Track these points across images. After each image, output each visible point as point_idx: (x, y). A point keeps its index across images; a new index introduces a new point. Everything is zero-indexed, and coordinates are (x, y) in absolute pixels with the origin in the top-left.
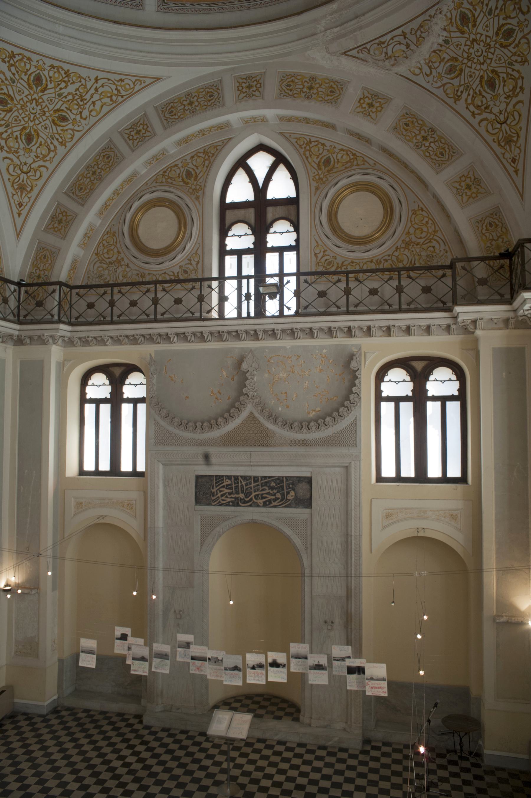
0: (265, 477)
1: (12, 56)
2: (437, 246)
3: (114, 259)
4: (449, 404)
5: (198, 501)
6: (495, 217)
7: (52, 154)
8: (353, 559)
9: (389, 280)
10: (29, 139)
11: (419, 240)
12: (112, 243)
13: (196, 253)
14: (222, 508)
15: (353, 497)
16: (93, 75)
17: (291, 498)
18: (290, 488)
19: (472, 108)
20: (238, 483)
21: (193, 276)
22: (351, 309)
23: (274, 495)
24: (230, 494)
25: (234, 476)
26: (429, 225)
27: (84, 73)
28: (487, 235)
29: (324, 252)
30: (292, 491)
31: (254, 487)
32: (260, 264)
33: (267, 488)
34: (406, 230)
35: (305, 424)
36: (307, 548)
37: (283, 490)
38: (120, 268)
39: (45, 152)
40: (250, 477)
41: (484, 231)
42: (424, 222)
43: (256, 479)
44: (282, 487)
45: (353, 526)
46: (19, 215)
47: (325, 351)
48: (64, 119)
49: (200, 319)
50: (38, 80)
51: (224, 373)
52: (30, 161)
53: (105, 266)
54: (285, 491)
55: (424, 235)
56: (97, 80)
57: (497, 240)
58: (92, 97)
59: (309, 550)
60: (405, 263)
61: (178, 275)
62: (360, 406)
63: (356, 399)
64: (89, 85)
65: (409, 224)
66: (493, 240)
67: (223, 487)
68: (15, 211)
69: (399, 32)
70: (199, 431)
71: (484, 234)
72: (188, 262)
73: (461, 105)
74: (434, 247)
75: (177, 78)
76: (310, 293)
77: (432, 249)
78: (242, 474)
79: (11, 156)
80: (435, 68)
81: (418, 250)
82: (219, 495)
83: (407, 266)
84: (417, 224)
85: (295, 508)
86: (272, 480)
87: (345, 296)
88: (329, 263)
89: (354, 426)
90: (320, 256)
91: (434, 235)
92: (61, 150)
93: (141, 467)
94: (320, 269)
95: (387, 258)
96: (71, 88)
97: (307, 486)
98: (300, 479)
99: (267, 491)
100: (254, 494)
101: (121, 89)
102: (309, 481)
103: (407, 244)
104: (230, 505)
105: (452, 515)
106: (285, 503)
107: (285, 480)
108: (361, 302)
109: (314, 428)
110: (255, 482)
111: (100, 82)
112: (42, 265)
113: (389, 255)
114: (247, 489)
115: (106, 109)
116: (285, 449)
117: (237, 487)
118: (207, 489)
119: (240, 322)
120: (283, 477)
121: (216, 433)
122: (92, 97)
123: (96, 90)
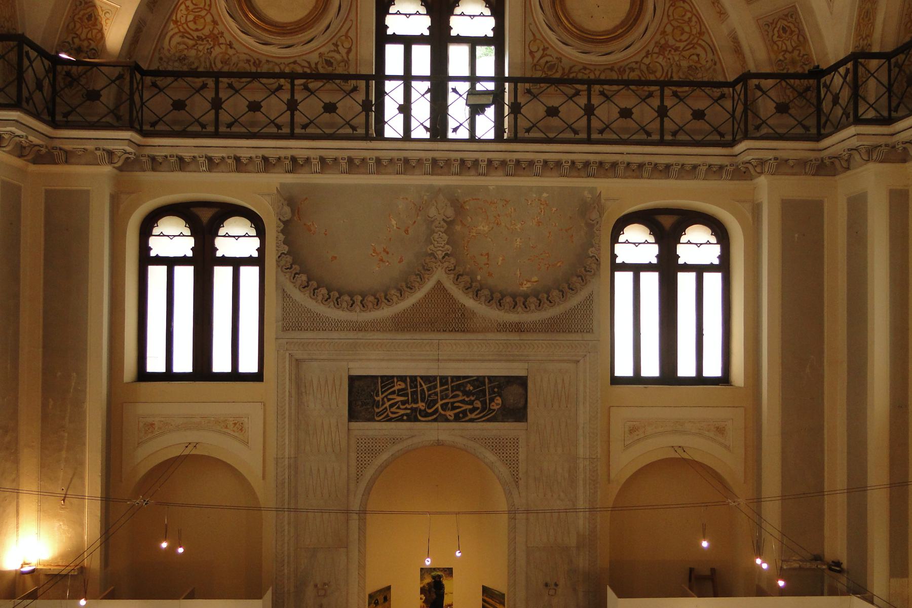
0: (458, 378)
2: (703, 55)
3: (206, 32)
4: (707, 276)
5: (353, 416)
6: (790, 19)
9: (720, 98)
11: (678, 44)
12: (202, 6)
13: (347, 36)
14: (392, 425)
17: (496, 407)
18: (494, 393)
20: (416, 386)
21: (340, 70)
22: (595, 136)
23: (471, 403)
24: (404, 403)
25: (411, 377)
26: (693, 23)
28: (780, 43)
29: (544, 50)
30: (498, 398)
31: (441, 391)
32: (439, 61)
34: (661, 29)
35: (519, 301)
37: (485, 395)
38: (217, 48)
40: (435, 377)
41: (775, 38)
42: (686, 18)
43: (444, 380)
44: (484, 391)
47: (545, 195)
49: (367, 137)
51: (394, 222)
53: (191, 43)
54: (487, 397)
55: (685, 37)
57: (793, 51)
60: (658, 74)
61: (317, 68)
63: (594, 266)
65: (665, 20)
66: (786, 51)
67: (393, 393)
70: (358, 309)
71: (775, 43)
72: (333, 48)
74: (698, 55)
76: (533, 110)
77: (695, 58)
78: (423, 374)
81: (677, 58)
82: (387, 404)
83: (662, 79)
84: (676, 20)
86: (468, 382)
87: (213, 111)
88: (552, 67)
90: (538, 55)
91: (699, 39)
93: (249, 364)
94: (538, 74)
95: (634, 66)
97: (521, 390)
99: (460, 398)
100: (440, 403)
102: (522, 382)
103: (663, 48)
104: (403, 421)
105: (718, 428)
108: (236, 121)
109: (533, 307)
110: (442, 385)
112: (85, 31)
113: (636, 63)
114: (429, 396)
116: (490, 336)
117: (415, 393)
118: (366, 397)
119: (474, 146)
120: (484, 377)
121: (386, 312)
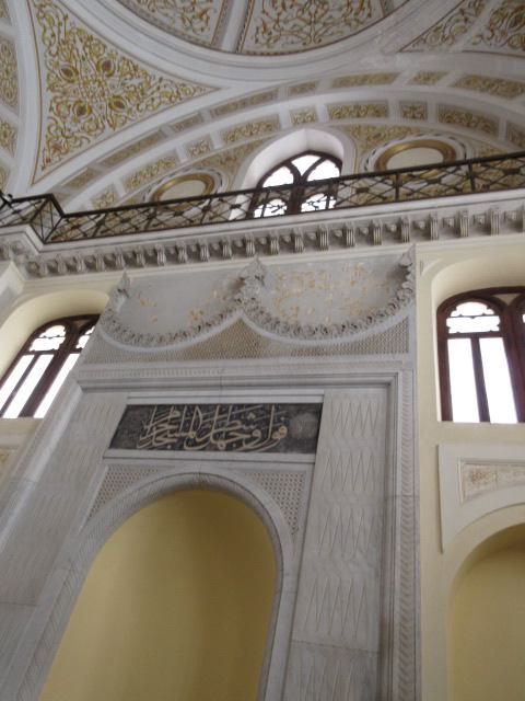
0: (240, 406)
1: (91, 38)
7: (98, 131)
8: (398, 549)
10: (81, 111)
15: (400, 426)
16: (158, 75)
18: (280, 421)
19: (54, 105)
20: (192, 415)
24: (172, 432)
27: (150, 71)
33: (239, 422)
36: (295, 530)
37: (268, 425)
39: (92, 126)
43: (224, 408)
44: (267, 421)
45: (399, 478)
46: (43, 168)
48: (121, 106)
50: (107, 65)
52: (74, 129)
54: (271, 425)
56: (161, 80)
58: (152, 93)
59: (299, 535)
62: (415, 302)
64: (152, 83)
68: (41, 163)
69: (458, 10)
73: (49, 95)
75: (235, 90)
79: (58, 119)
80: (498, 28)
82: (155, 433)
85: (285, 452)
89: (405, 325)
92: (108, 130)
96: (136, 82)
98: (301, 408)
100: (214, 431)
101: (181, 91)
102: (317, 410)
106: (267, 443)
107: (273, 409)
111: (163, 83)
114: (203, 425)
115: (162, 106)
122: (152, 93)
123: (159, 88)
